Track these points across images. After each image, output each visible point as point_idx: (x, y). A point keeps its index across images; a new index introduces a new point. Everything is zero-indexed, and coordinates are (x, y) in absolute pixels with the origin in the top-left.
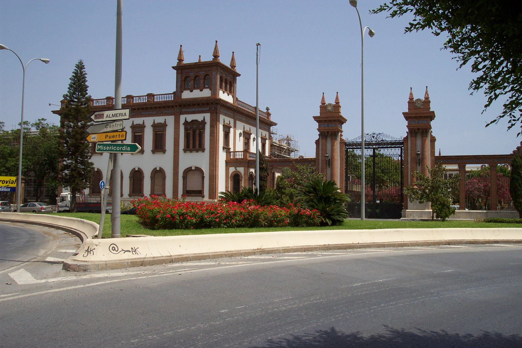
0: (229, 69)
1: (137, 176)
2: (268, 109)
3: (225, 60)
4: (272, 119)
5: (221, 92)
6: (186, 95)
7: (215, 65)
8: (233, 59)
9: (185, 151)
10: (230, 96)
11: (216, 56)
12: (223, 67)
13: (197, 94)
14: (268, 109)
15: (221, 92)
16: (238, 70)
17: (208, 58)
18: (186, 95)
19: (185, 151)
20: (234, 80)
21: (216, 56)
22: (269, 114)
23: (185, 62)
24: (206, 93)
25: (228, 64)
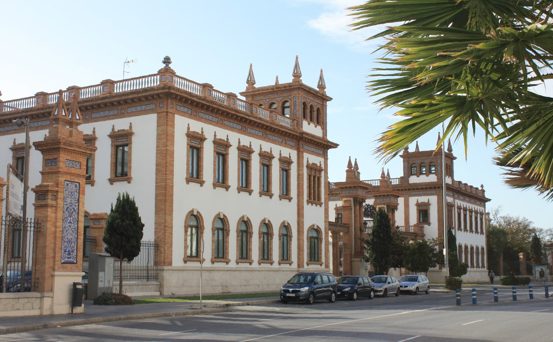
0: (317, 92)
1: (195, 221)
2: (482, 186)
3: (310, 81)
4: (487, 195)
5: (305, 123)
6: (413, 180)
7: (297, 86)
8: (321, 78)
9: (308, 202)
10: (319, 128)
11: (297, 75)
12: (308, 91)
13: (423, 179)
14: (482, 186)
15: (305, 123)
16: (328, 92)
17: (287, 79)
18: (413, 180)
19: (308, 202)
20: (324, 107)
21: (297, 75)
22: (483, 191)
23: (257, 86)
24: (433, 178)
25: (313, 84)
